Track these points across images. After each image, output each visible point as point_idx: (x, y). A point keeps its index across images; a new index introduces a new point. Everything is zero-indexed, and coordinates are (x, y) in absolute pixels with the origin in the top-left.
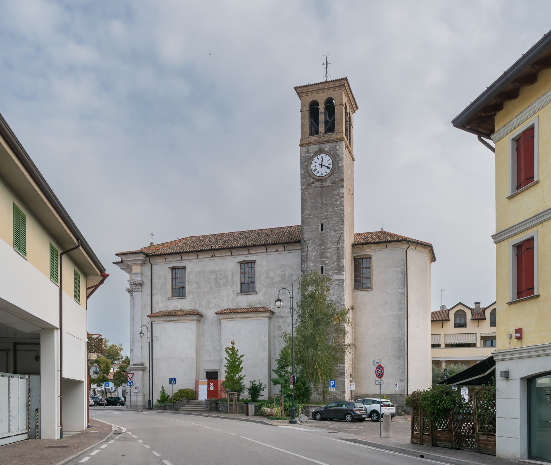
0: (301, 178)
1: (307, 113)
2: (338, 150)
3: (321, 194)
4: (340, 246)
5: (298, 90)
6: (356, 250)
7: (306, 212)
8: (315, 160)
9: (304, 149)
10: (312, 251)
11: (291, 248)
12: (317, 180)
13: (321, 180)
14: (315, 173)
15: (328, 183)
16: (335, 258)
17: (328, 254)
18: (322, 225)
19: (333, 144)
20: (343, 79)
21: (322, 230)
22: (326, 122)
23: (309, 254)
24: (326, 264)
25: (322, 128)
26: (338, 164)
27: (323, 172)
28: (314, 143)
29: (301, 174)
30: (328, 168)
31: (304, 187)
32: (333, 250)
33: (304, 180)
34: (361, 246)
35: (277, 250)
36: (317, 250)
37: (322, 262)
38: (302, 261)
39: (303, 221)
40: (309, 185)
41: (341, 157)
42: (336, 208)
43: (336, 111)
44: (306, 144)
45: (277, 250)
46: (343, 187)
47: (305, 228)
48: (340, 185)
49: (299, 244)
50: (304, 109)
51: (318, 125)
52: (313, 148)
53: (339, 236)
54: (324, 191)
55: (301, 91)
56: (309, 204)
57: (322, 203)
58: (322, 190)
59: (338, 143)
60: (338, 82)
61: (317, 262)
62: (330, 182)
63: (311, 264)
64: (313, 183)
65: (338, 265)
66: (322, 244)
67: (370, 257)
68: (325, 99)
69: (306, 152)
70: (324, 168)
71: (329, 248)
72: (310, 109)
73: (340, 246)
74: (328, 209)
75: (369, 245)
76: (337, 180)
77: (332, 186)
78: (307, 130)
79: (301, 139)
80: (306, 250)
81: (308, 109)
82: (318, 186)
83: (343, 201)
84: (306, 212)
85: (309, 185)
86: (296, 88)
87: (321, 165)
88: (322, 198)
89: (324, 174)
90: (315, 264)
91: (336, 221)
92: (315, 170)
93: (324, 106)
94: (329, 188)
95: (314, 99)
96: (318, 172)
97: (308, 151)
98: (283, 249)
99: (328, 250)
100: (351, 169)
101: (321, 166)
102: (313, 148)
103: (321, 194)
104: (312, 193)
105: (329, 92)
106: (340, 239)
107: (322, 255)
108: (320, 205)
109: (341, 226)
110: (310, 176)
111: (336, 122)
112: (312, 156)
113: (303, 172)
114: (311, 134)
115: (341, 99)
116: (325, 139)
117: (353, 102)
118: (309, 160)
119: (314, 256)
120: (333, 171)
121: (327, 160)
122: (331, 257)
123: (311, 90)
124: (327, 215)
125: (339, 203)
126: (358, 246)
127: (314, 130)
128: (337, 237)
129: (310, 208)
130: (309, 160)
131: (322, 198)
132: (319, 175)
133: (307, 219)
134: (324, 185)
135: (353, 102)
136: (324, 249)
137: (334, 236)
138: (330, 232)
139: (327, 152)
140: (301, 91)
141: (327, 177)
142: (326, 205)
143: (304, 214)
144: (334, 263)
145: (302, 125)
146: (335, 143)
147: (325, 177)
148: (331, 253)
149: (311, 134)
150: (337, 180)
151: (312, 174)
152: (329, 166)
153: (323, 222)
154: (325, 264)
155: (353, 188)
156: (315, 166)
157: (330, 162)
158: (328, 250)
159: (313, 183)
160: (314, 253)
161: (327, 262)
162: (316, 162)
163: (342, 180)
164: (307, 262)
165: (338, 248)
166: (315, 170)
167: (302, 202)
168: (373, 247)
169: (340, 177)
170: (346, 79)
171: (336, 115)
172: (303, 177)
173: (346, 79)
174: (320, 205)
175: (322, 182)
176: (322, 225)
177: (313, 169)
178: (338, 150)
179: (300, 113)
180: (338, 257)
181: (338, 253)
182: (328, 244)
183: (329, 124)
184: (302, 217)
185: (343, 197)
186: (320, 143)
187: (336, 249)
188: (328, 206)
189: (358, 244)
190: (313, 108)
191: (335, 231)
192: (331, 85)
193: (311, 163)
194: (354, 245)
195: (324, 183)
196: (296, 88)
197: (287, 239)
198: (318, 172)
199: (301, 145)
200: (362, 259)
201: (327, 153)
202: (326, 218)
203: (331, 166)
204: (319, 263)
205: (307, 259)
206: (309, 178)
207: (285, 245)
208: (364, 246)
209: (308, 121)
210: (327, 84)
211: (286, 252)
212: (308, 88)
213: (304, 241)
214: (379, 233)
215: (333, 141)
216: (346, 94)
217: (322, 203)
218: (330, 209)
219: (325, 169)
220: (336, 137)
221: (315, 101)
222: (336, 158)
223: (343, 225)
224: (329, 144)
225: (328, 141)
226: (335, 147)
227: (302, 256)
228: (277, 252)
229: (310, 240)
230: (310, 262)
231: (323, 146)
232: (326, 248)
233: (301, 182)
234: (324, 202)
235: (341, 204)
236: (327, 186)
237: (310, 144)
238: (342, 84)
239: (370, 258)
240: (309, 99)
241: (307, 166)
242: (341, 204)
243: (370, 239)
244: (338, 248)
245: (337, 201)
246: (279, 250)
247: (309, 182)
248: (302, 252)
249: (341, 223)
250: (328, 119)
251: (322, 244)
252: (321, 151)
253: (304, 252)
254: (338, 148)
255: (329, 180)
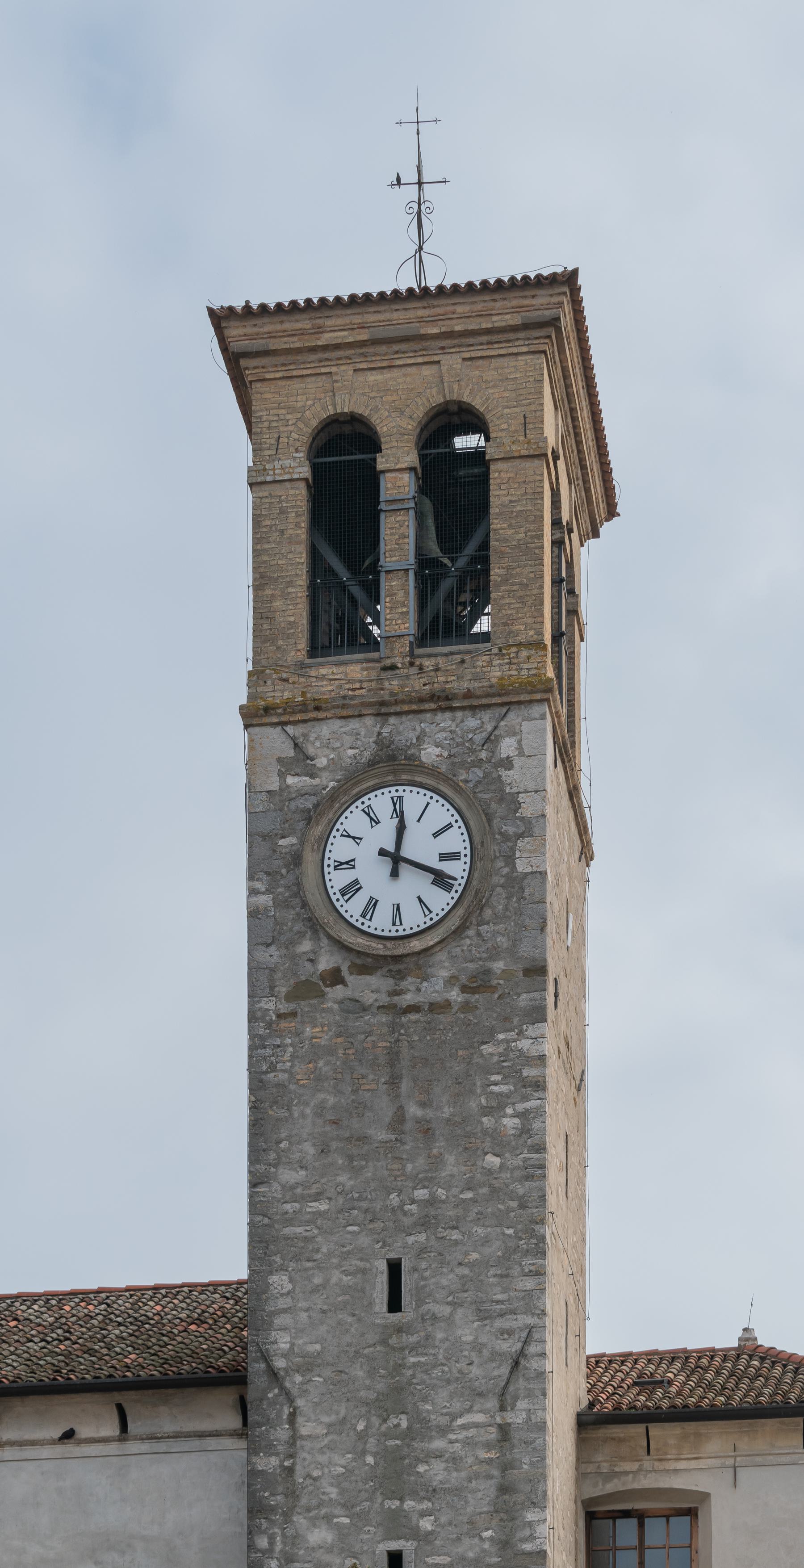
0: (256, 941)
1: (298, 498)
2: (507, 764)
3: (393, 1056)
4: (516, 1417)
5: (234, 331)
6: (602, 1458)
7: (288, 1176)
8: (353, 820)
9: (277, 742)
10: (323, 1440)
11: (168, 1419)
12: (366, 963)
13: (394, 959)
14: (353, 909)
15: (437, 984)
16: (481, 1498)
17: (435, 1472)
18: (395, 1269)
19: (472, 723)
20: (553, 280)
21: (395, 1305)
22: (427, 572)
23: (307, 1462)
24: (424, 1539)
25: (396, 611)
26: (510, 860)
27: (404, 905)
28: (346, 709)
29: (253, 914)
30: (441, 880)
31: (269, 1005)
32: (468, 1443)
33: (272, 955)
34: (639, 1429)
35: (69, 1435)
36: (362, 1436)
37: (396, 1523)
38: (257, 1510)
39: (262, 1241)
40: (306, 990)
41: (527, 811)
42: (493, 1161)
43: (498, 497)
44: (288, 707)
45: (69, 1435)
46: (538, 1015)
47: (279, 1282)
48: (524, 1000)
49: (229, 1396)
50: (277, 469)
51: (373, 593)
52: (339, 743)
53: (510, 1346)
54: (405, 1039)
55: (254, 344)
56: (303, 1126)
57: (400, 1118)
58: (393, 1027)
59: (513, 718)
60: (514, 300)
61: (360, 1519)
62: (451, 981)
63: (319, 1536)
64: (335, 977)
65: (504, 1544)
66: (395, 1397)
67: (689, 1510)
68: (420, 410)
69: (286, 767)
70: (413, 884)
71: (443, 1431)
72: (316, 468)
73: (516, 1417)
74: (437, 1162)
75: (691, 1427)
76: (498, 966)
77: (466, 1007)
78: (295, 611)
79: (256, 676)
80: (282, 1433)
81: (305, 471)
82: (369, 998)
83: (540, 1112)
84: (288, 1176)
85: (306, 990)
86: (221, 318)
87: (396, 860)
88: (394, 1082)
89: (413, 920)
90: (342, 1533)
91: (495, 1249)
92: (352, 889)
93: (411, 458)
94: (444, 1019)
95: (345, 405)
96: (373, 904)
97: (301, 760)
98: (111, 1429)
99: (439, 1444)
100: (576, 905)
101: (391, 862)
102: (339, 743)
103: (393, 1056)
104: (331, 1051)
105: (452, 362)
106: (522, 1365)
107: (395, 1474)
108: (383, 1135)
109: (529, 1284)
110: (314, 926)
111: (496, 572)
112: (334, 796)
113: (265, 900)
114: (318, 648)
115: (531, 422)
116: (417, 685)
117: (592, 460)
118: (309, 818)
119: (338, 1481)
120: (472, 904)
121: (434, 828)
122: (457, 1491)
123: (326, 338)
124: (432, 1201)
125: (510, 1123)
126: (617, 1431)
127: (337, 617)
128: (496, 1355)
129: (310, 1149)
130: (309, 818)
131: (394, 1082)
132: (381, 923)
133: (289, 1221)
134: (409, 998)
135: (592, 460)
136: (408, 1435)
137: (477, 1347)
138: (449, 1321)
139: (432, 771)
140: (254, 344)
141: (430, 940)
142: (427, 1131)
143: (274, 1190)
144: (473, 1529)
145: (263, 580)
146: (486, 716)
147: (416, 945)
148: (455, 1461)
149: (318, 648)
150: (498, 966)
151: (322, 914)
152: (448, 867)
153: (404, 1247)
154: (415, 1534)
155: (582, 1041)
156: (350, 864)
157: (456, 840)
158: (439, 1444)
159: (335, 977)
160: (340, 1462)
161: (426, 1524)
162: (358, 838)
163: (537, 970)
164: (287, 1516)
165: (504, 1430)
166: (352, 889)
167: (255, 1107)
168: (718, 1440)
169: (525, 950)
170: (568, 280)
171: (496, 524)
172: (262, 930)
173: (568, 280)
174: (383, 1135)
175: (400, 976)
176: (395, 1269)
177: (337, 880)
178: (507, 764)
179: (243, 501)
180: (504, 1489)
181: (506, 1467)
182: (439, 1403)
183: (447, 584)
184: (256, 1207)
185: (539, 1085)
186: (383, 709)
187: (493, 1434)
188: (439, 1145)
189: (618, 1418)
190: (341, 462)
191: (484, 1316)
192: (461, 316)
193: (324, 841)
194: (588, 1423)
195: (409, 982)
196: (221, 318)
197: (131, 1360)
198: (373, 904)
199: (254, 716)
200: (641, 1517)
201: (436, 781)
202: (425, 1223)
203: (458, 870)
204: (371, 1532)
205: (292, 1494)
206: (306, 946)
207: (127, 1398)
208: (656, 1430)
209: (300, 556)
210: (443, 307)
211: (133, 1447)
212: (303, 323)
213: (273, 1374)
214: (725, 1354)
215: (474, 703)
216: (561, 392)
217: (400, 1118)
218: (452, 1165)
219: (423, 885)
220: (495, 674)
221: (354, 419)
222: (495, 820)
223: (539, 1273)
224: (445, 720)
225: (442, 701)
226: (491, 741)
227: (253, 1473)
228: (69, 1449)
229: (308, 1365)
230: (314, 1522)
231: (404, 730)
232: (420, 1429)
233: (254, 968)
234: (413, 1110)
235: (525, 1131)
236: (436, 1008)
237: (313, 709)
238: (543, 313)
239: (691, 1513)
240: (307, 402)
241: (296, 859)
242: (525, 1131)
243: (680, 1388)
244: (504, 1430)
245: (496, 1108)
246: (84, 1431)
247: (306, 971)
248: (253, 1451)
249: (528, 1263)
250: (434, 549)
251: (395, 1397)
252: (392, 766)
253: (270, 1449)
254: (507, 747)
255: (442, 969)
